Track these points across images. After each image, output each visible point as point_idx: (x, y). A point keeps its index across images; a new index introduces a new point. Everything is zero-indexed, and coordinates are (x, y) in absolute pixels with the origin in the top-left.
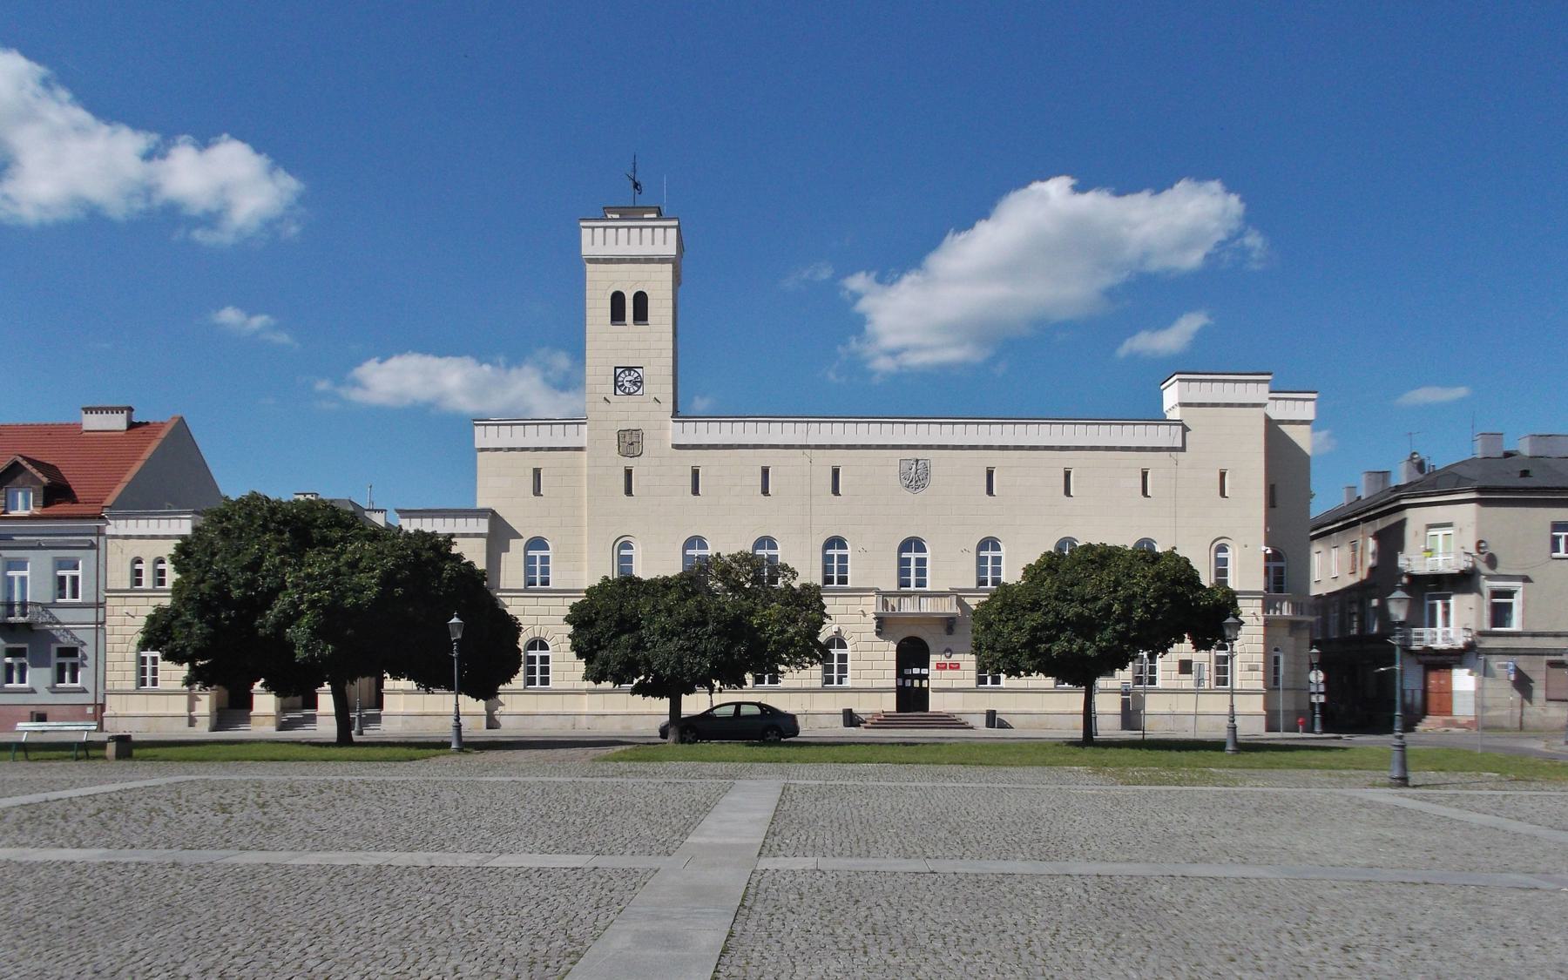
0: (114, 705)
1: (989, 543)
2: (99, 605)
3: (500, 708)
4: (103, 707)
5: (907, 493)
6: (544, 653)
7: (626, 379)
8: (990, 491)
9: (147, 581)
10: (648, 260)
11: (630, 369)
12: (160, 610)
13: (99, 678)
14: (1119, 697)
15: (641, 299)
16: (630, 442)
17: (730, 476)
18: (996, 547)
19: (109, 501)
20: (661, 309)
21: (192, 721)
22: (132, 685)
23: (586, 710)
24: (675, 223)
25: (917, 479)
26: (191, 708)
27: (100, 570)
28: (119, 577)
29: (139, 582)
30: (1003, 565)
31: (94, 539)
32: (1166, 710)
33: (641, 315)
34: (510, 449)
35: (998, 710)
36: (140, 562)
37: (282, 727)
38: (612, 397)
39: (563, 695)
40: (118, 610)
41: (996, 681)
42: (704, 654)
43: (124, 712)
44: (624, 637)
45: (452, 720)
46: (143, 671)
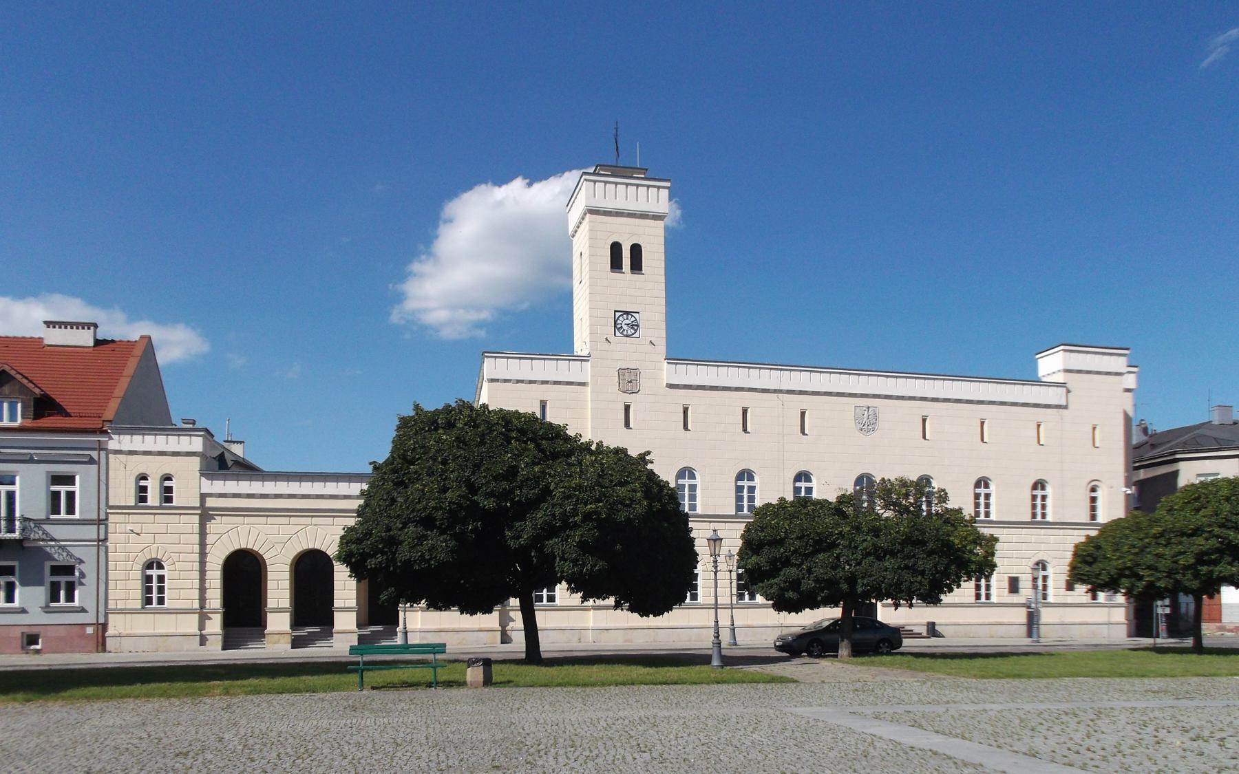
0: (116, 625)
1: (745, 474)
2: (101, 522)
3: (511, 624)
4: (105, 626)
5: (858, 434)
6: (160, 572)
7: (624, 322)
8: (627, 425)
9: (153, 497)
10: (644, 216)
11: (627, 313)
12: (350, 530)
13: (102, 596)
14: (1024, 611)
15: (636, 250)
16: (629, 380)
17: (897, 420)
18: (692, 476)
19: (109, 414)
20: (654, 259)
21: (203, 640)
22: (138, 604)
23: (591, 625)
24: (668, 184)
25: (868, 425)
26: (202, 626)
27: (103, 484)
28: (122, 492)
29: (143, 499)
30: (698, 492)
31: (94, 454)
32: (1056, 621)
33: (636, 266)
34: (518, 381)
35: (937, 621)
36: (144, 478)
37: (297, 643)
38: (612, 338)
39: (719, 609)
40: (120, 528)
41: (752, 597)
42: (922, 573)
43: (128, 632)
44: (821, 556)
45: (712, 632)
46: (149, 590)
